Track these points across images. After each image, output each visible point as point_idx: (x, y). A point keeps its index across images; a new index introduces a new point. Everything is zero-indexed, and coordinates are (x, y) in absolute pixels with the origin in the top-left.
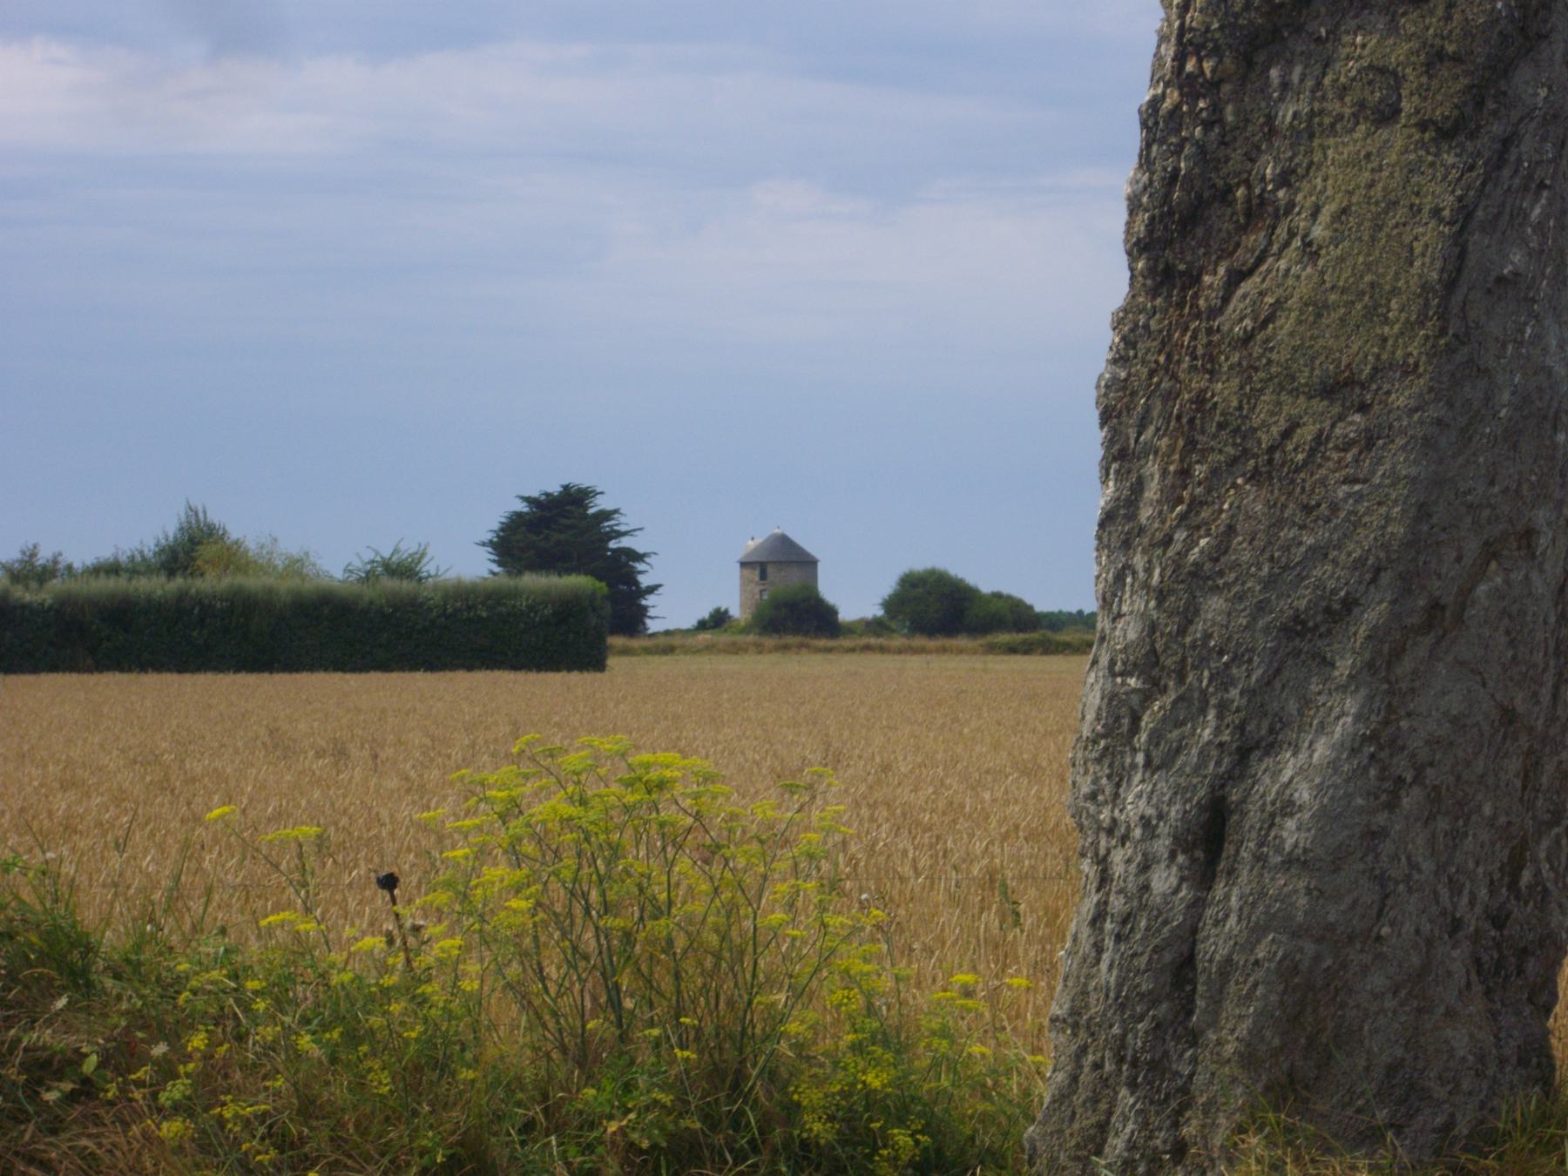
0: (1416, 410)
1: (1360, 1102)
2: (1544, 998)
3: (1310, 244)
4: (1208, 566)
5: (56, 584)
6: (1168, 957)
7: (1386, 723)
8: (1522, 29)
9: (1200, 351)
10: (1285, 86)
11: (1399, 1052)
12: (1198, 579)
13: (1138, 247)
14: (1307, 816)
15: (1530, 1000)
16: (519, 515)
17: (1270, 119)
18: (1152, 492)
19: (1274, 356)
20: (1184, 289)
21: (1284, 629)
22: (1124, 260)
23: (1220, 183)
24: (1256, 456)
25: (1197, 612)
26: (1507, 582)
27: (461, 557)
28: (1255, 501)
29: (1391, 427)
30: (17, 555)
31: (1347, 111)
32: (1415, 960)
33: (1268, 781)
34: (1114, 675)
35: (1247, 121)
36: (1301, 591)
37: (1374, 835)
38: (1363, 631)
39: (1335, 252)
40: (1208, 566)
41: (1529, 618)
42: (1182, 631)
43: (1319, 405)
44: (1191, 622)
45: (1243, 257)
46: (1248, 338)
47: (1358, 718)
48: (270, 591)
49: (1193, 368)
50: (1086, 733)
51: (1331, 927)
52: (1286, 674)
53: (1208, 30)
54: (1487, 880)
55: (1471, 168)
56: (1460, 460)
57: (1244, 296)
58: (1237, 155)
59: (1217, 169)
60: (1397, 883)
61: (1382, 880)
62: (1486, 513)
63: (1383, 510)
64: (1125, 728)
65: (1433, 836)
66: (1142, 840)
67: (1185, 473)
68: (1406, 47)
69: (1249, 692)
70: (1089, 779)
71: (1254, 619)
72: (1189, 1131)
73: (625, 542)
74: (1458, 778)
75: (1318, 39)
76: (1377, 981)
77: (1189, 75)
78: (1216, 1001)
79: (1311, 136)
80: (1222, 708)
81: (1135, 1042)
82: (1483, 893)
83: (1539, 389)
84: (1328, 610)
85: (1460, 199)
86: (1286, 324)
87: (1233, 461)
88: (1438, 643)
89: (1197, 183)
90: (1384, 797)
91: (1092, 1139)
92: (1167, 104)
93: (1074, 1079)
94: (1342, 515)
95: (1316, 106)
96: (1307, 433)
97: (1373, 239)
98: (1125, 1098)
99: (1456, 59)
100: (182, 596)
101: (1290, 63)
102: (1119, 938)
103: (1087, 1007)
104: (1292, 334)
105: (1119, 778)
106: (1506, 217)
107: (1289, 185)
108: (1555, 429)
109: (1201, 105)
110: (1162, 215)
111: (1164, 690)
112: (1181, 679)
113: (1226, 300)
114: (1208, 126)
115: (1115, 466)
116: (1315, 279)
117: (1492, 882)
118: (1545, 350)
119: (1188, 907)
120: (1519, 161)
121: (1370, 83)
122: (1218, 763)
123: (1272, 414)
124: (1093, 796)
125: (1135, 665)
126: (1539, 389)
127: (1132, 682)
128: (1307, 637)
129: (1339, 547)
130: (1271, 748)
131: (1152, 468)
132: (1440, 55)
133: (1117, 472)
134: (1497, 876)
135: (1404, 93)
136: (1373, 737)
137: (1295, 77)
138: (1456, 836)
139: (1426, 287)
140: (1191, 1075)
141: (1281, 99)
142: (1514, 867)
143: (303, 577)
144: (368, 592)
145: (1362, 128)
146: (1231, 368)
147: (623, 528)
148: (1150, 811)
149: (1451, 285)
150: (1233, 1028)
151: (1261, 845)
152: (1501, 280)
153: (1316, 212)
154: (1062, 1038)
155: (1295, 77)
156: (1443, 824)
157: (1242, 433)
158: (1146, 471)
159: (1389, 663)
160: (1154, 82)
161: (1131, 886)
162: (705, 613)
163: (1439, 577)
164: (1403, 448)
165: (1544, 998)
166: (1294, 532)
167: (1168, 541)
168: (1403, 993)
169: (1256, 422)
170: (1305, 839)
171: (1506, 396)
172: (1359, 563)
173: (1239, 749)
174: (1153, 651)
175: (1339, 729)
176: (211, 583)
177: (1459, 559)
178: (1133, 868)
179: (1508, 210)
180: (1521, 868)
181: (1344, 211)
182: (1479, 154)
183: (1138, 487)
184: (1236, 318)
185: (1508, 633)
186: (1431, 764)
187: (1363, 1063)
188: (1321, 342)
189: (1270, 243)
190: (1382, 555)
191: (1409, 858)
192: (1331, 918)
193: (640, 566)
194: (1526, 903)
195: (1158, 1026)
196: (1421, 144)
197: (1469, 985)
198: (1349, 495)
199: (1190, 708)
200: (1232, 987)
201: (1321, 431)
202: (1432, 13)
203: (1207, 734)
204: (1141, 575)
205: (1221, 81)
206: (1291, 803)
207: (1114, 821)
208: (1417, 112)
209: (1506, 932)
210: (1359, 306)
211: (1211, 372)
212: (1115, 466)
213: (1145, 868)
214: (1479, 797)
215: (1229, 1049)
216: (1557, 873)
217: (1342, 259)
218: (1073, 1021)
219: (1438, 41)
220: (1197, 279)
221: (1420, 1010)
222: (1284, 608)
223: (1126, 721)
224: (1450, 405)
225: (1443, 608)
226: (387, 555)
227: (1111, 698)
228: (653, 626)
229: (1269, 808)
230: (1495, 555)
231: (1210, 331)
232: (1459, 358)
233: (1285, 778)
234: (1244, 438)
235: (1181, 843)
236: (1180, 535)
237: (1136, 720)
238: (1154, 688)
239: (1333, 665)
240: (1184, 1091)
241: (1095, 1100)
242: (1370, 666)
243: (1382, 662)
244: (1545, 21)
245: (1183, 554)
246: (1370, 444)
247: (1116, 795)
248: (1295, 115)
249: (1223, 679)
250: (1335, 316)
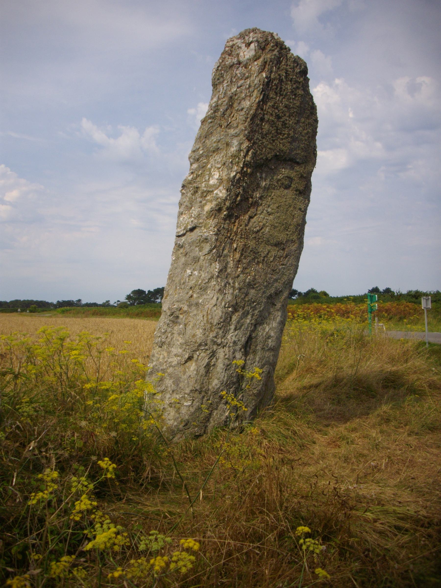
46: (258, 231)
47: (281, 317)
77: (245, 172)
91: (207, 417)
113: (248, 223)
127: (230, 309)
129: (280, 279)
170: (274, 344)
202: (302, 167)
203: (248, 321)
222: (268, 294)
237: (231, 318)
238: (235, 310)
239: (276, 305)
249: (254, 308)
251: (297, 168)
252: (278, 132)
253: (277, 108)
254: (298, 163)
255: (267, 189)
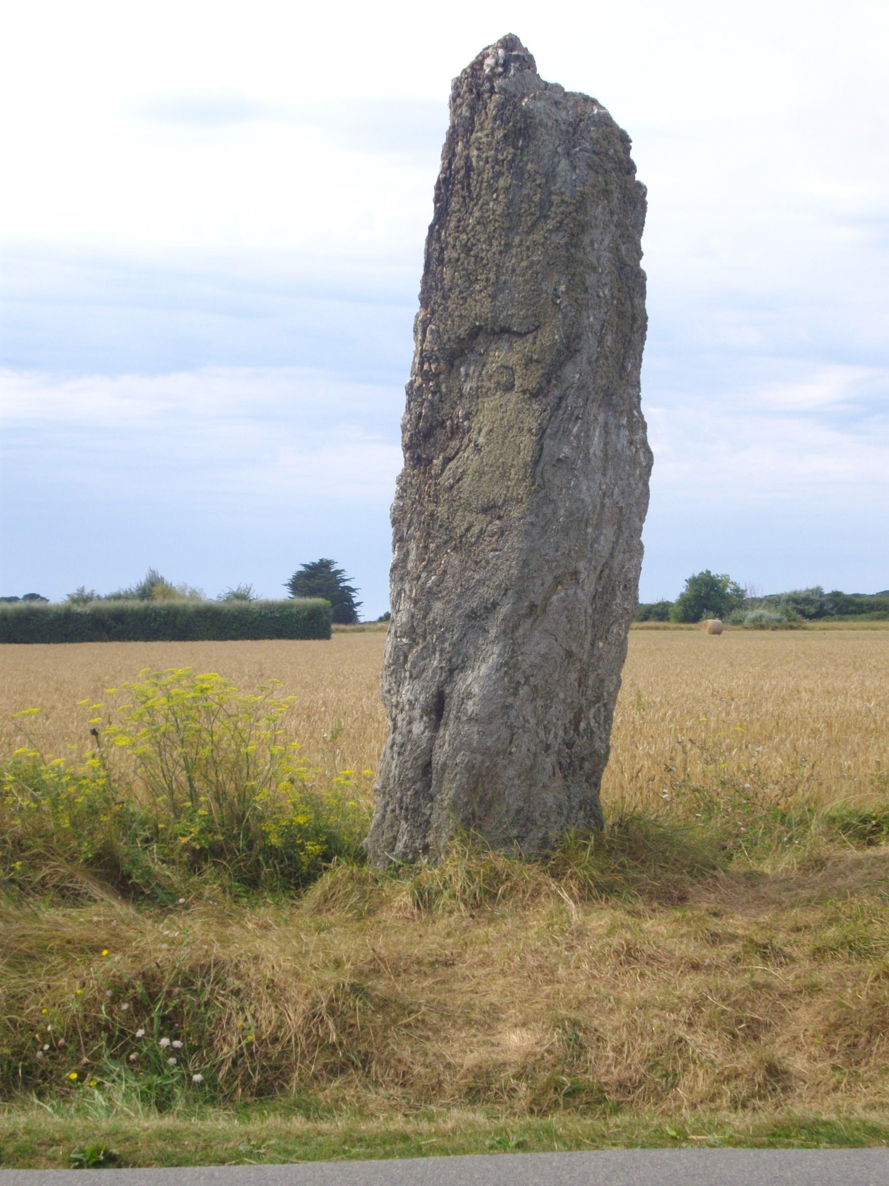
0: (522, 518)
1: (504, 826)
2: (594, 779)
3: (477, 445)
4: (435, 588)
5: (92, 604)
6: (420, 762)
7: (512, 657)
8: (568, 348)
9: (432, 493)
10: (467, 375)
11: (521, 804)
12: (430, 594)
13: (407, 447)
14: (477, 699)
15: (586, 781)
16: (301, 572)
17: (460, 389)
18: (412, 556)
19: (462, 495)
20: (426, 466)
21: (467, 616)
22: (402, 453)
23: (440, 419)
24: (455, 540)
25: (430, 609)
26: (566, 594)
27: (272, 588)
28: (455, 560)
29: (511, 526)
30: (75, 591)
31: (492, 386)
32: (528, 763)
33: (461, 683)
34: (397, 637)
35: (451, 391)
36: (474, 599)
37: (507, 707)
38: (500, 617)
39: (487, 449)
40: (435, 588)
41: (577, 610)
42: (424, 618)
43: (481, 517)
44: (428, 613)
45: (450, 452)
46: (451, 487)
47: (499, 655)
48: (185, 606)
49: (429, 501)
50: (386, 663)
51: (489, 748)
52: (469, 636)
53: (433, 351)
54: (563, 727)
55: (545, 411)
56: (542, 540)
57: (450, 469)
58: (447, 407)
59: (439, 413)
60: (518, 728)
61: (511, 727)
62: (554, 564)
63: (508, 563)
64: (401, 661)
65: (535, 707)
66: (409, 710)
67: (426, 547)
68: (516, 356)
69: (453, 645)
70: (387, 683)
71: (454, 612)
72: (430, 839)
73: (347, 584)
74: (546, 682)
75: (480, 354)
76: (510, 772)
77: (426, 371)
78: (440, 782)
79: (478, 397)
80: (442, 651)
81: (407, 800)
82: (561, 733)
83: (578, 509)
84: (486, 608)
85: (540, 424)
86: (467, 481)
87: (446, 542)
88: (535, 621)
89: (430, 419)
90: (511, 690)
91: (391, 843)
92: (417, 384)
93: (384, 817)
94: (491, 565)
95: (480, 384)
96: (476, 530)
97: (503, 442)
98: (404, 825)
99: (538, 361)
100: (146, 608)
101: (469, 365)
102: (399, 754)
103: (389, 785)
104: (469, 485)
105: (399, 683)
106: (561, 432)
107: (469, 419)
108: (586, 526)
109: (431, 384)
110: (416, 433)
111: (418, 644)
112: (425, 638)
113: (443, 471)
114: (434, 393)
115: (398, 545)
116: (479, 461)
117: (565, 728)
118: (580, 491)
119: (428, 740)
120: (567, 407)
121: (502, 373)
122: (440, 676)
123: (462, 521)
124: (389, 691)
125: (405, 633)
126: (578, 509)
127: (404, 640)
128: (475, 619)
129: (489, 579)
130: (463, 669)
131: (413, 545)
132: (531, 360)
133: (399, 547)
134: (568, 725)
135: (516, 377)
136: (506, 664)
137: (471, 372)
138: (547, 707)
139: (525, 464)
140: (430, 815)
141: (465, 381)
142: (576, 721)
143: (199, 599)
144: (228, 607)
145: (499, 393)
146: (445, 501)
147: (345, 578)
148: (412, 698)
149: (536, 462)
150: (447, 793)
151: (458, 712)
152: (559, 460)
153: (480, 430)
154: (379, 799)
155: (471, 372)
156: (540, 702)
157: (449, 530)
158: (410, 547)
159: (513, 631)
160: (413, 373)
161: (404, 731)
162: (382, 614)
163: (534, 592)
164: (516, 535)
165: (594, 779)
166: (471, 573)
167: (419, 577)
168: (523, 778)
169: (455, 525)
170: (476, 709)
171: (562, 512)
172: (498, 587)
173: (449, 670)
174: (413, 626)
175: (491, 660)
176: (159, 603)
177: (543, 585)
178: (405, 723)
179: (562, 429)
180: (579, 722)
181: (491, 431)
182: (548, 404)
183: (407, 554)
184: (446, 480)
185: (567, 617)
186: (533, 676)
187: (505, 809)
188: (481, 489)
189: (461, 445)
190: (508, 583)
191: (524, 717)
192: (489, 744)
193: (353, 594)
194: (583, 737)
195: (416, 793)
196: (524, 400)
197: (554, 774)
198: (494, 556)
199: (428, 652)
200: (446, 775)
201: (482, 528)
203: (436, 663)
204: (408, 593)
205: (440, 373)
206: (470, 693)
207: (398, 702)
208: (521, 385)
209: (573, 750)
210: (497, 473)
211: (436, 503)
212: (398, 545)
213: (410, 723)
214: (557, 690)
215: (446, 803)
216: (599, 724)
217: (490, 452)
218: (383, 790)
219: (530, 354)
220: (431, 462)
221: (531, 785)
223: (402, 658)
224: (537, 516)
225: (536, 606)
226: (235, 590)
227: (395, 647)
228: (362, 619)
229: (461, 696)
230: (560, 583)
231: (436, 485)
232: (541, 495)
233: (468, 683)
234: (450, 531)
235: (425, 712)
236: (424, 575)
237: (406, 657)
238: (414, 642)
239: (488, 632)
240: (428, 822)
241: (392, 826)
242: (504, 632)
243: (509, 630)
244: (578, 344)
245: (424, 583)
246: (502, 534)
247: (398, 691)
248: (471, 388)
249: (442, 639)
250: (487, 477)
251: (517, 346)
252: (470, 279)
253: (464, 230)
254: (520, 335)
255: (476, 394)
